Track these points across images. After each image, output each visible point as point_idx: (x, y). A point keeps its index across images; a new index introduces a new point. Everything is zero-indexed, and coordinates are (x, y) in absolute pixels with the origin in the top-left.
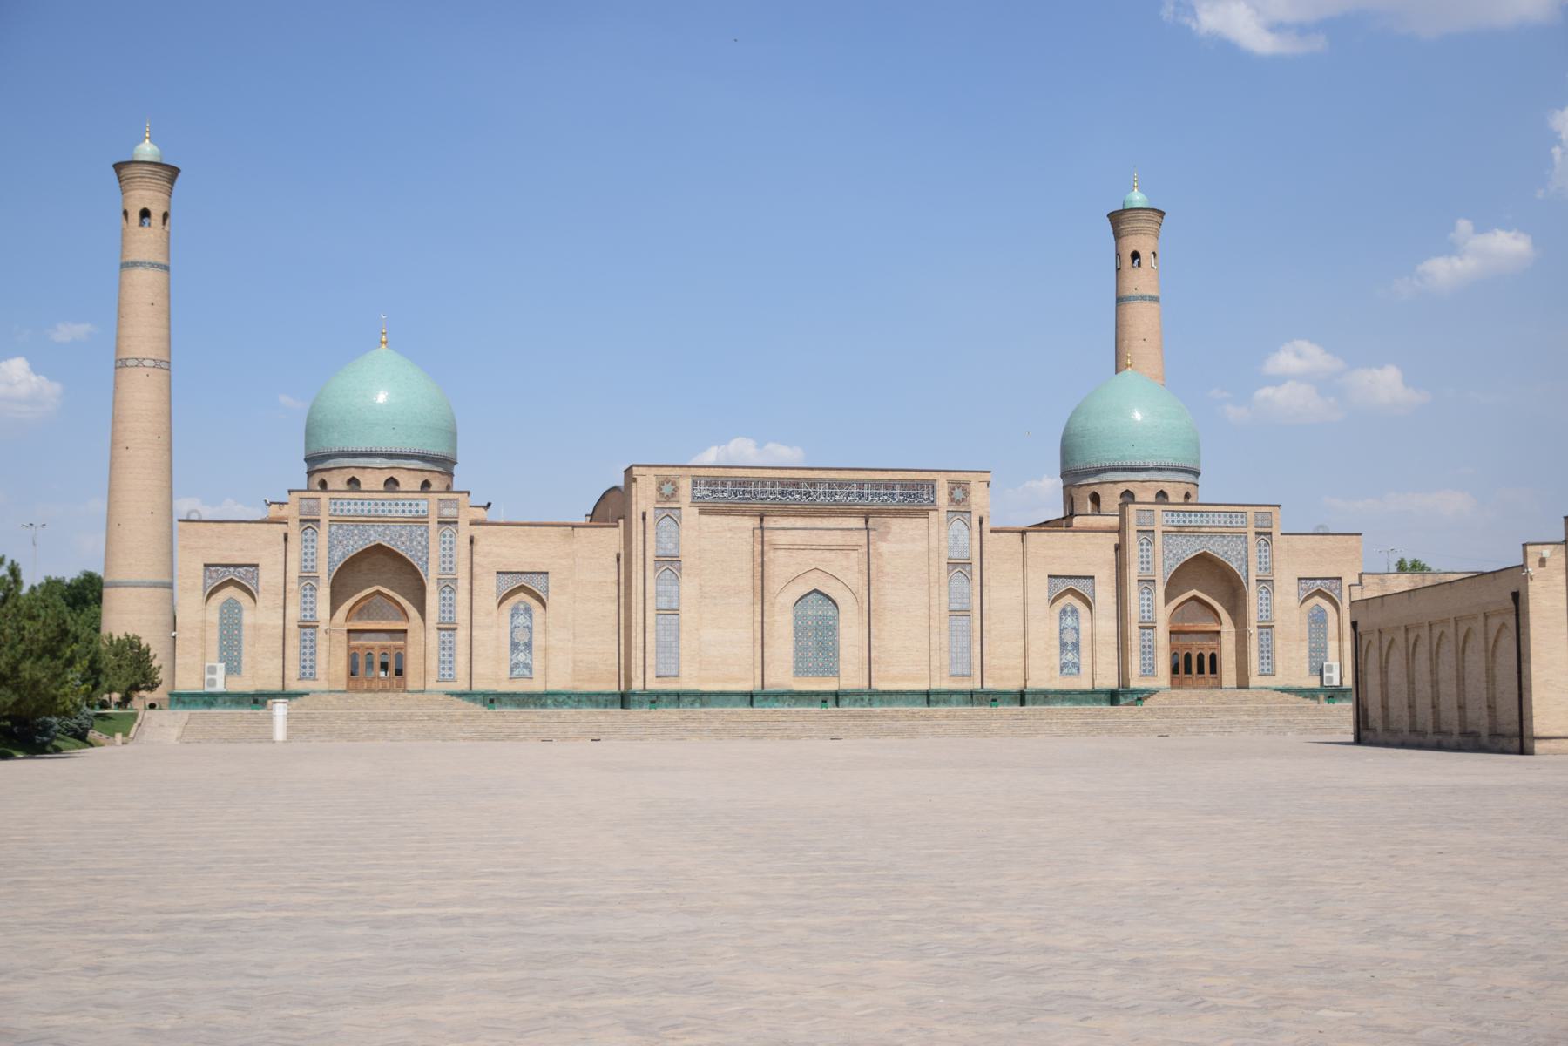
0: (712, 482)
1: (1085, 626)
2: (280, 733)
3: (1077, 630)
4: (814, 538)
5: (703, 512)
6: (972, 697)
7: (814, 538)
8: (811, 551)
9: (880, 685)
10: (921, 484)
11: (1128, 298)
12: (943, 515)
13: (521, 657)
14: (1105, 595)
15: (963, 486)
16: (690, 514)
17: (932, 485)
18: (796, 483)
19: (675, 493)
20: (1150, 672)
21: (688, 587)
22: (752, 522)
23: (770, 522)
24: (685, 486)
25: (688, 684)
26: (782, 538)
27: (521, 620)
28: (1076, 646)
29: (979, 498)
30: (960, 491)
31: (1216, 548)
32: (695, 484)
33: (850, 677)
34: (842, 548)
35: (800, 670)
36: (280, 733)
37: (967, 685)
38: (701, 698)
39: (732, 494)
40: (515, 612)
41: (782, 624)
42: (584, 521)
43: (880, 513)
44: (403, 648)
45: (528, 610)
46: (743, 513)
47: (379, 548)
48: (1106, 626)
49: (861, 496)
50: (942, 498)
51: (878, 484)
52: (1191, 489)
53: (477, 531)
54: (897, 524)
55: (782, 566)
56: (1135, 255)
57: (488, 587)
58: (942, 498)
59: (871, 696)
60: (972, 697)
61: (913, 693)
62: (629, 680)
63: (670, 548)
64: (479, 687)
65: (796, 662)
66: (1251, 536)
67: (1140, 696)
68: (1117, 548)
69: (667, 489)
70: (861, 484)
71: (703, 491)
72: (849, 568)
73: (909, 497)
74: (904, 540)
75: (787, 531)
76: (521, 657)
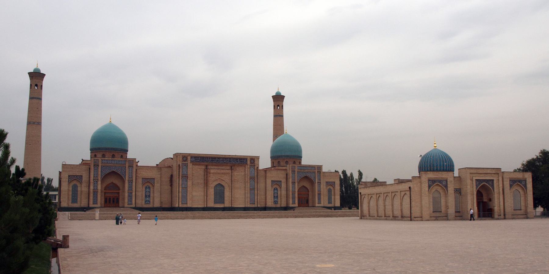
1: (279, 192)
3: (150, 192)
7: (219, 171)
8: (217, 175)
13: (148, 199)
14: (284, 185)
16: (190, 165)
20: (95, 202)
21: (190, 183)
24: (189, 158)
26: (212, 171)
28: (277, 197)
32: (191, 157)
33: (227, 204)
35: (215, 202)
37: (253, 206)
41: (211, 191)
48: (284, 192)
50: (249, 162)
55: (212, 178)
57: (140, 181)
58: (249, 162)
66: (127, 167)
67: (293, 208)
69: (185, 159)
75: (213, 170)
76: (148, 199)
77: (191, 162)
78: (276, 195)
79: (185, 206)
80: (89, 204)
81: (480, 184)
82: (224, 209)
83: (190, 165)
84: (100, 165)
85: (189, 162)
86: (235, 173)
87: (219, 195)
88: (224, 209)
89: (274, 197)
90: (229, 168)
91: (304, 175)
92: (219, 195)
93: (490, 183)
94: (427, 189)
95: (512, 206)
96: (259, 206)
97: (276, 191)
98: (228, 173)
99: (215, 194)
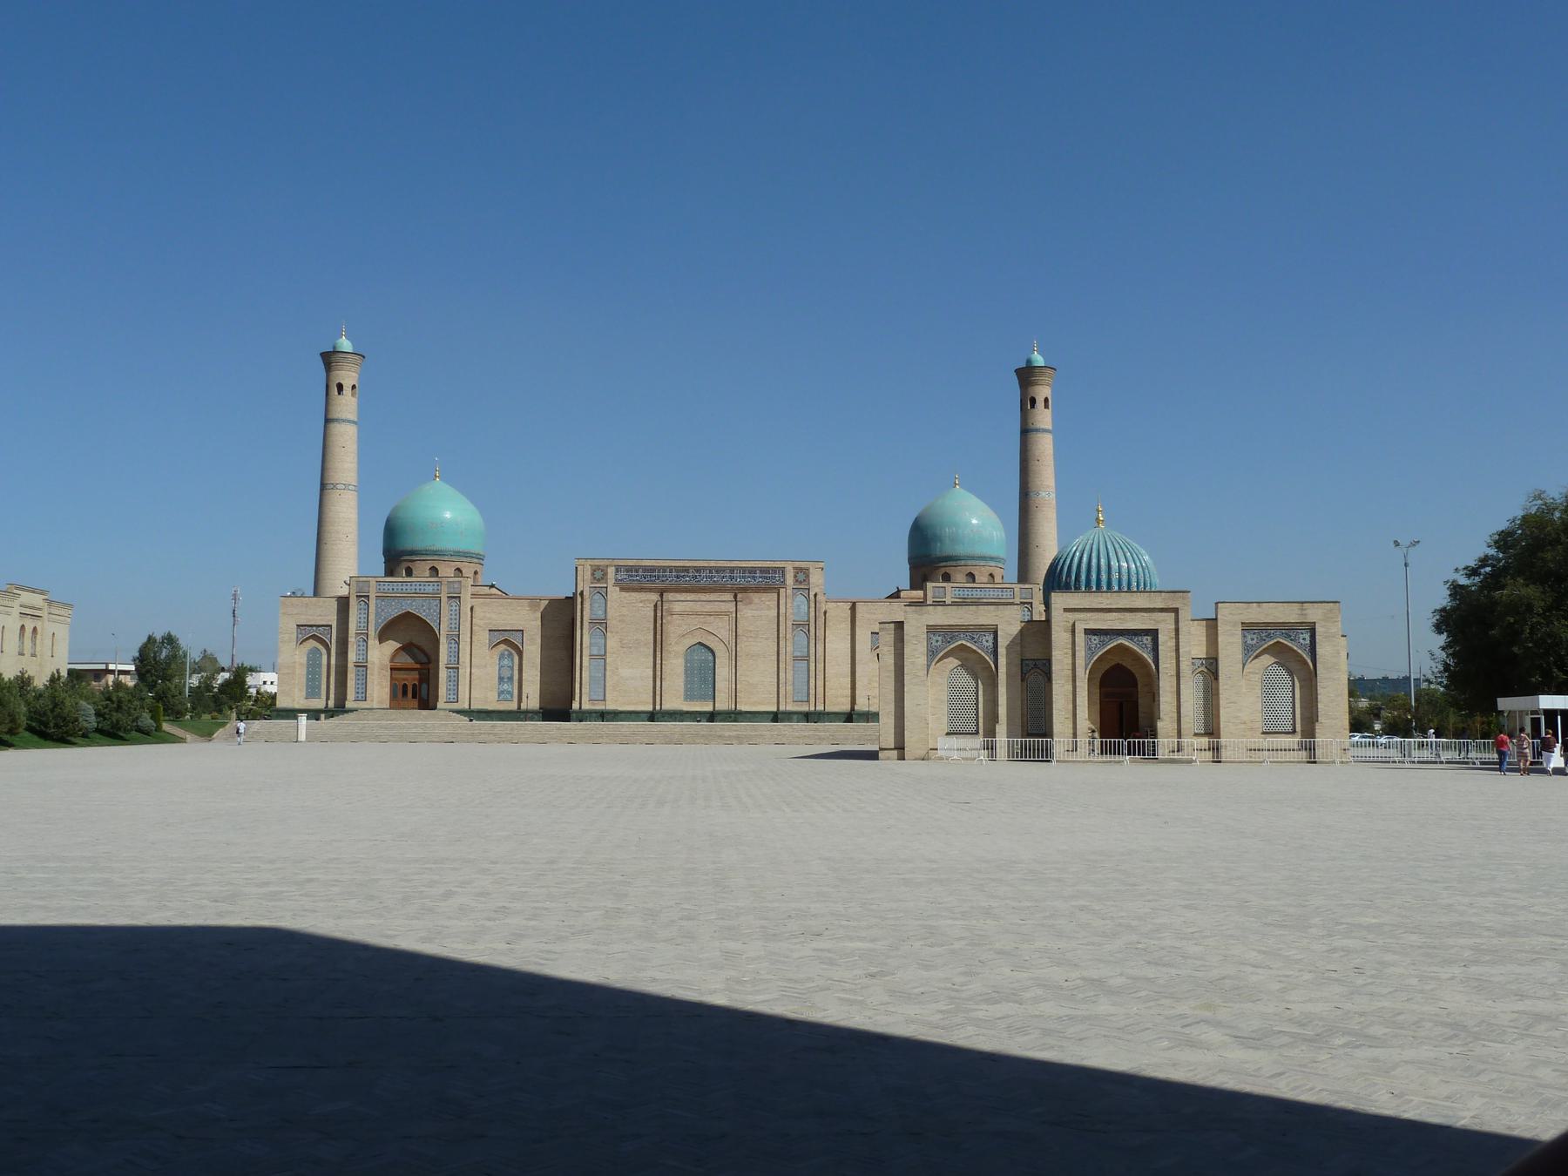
0: (629, 569)
2: (302, 737)
4: (698, 607)
5: (622, 589)
6: (808, 717)
7: (698, 607)
8: (692, 617)
9: (742, 707)
10: (775, 570)
11: (337, 420)
12: (789, 591)
13: (506, 687)
15: (805, 571)
16: (614, 593)
17: (783, 570)
18: (686, 569)
19: (604, 577)
21: (612, 642)
22: (655, 597)
23: (669, 596)
24: (611, 571)
25: (611, 706)
26: (677, 607)
27: (506, 662)
29: (816, 579)
30: (802, 574)
33: (723, 704)
34: (718, 614)
35: (689, 697)
36: (302, 737)
37: (805, 708)
38: (615, 716)
39: (639, 578)
40: (502, 657)
41: (675, 666)
43: (745, 590)
45: (510, 655)
46: (650, 590)
47: (408, 616)
49: (732, 578)
50: (790, 580)
51: (744, 569)
52: (478, 568)
53: (475, 602)
54: (755, 597)
56: (340, 387)
57: (483, 637)
58: (790, 580)
59: (734, 716)
60: (808, 717)
61: (700, 713)
62: (853, 702)
63: (600, 613)
65: (686, 691)
66: (444, 599)
69: (598, 574)
70: (732, 570)
72: (722, 628)
73: (766, 580)
74: (759, 611)
75: (680, 603)
76: (506, 687)
77: (618, 582)
78: (507, 674)
79: (599, 707)
80: (853, 702)
81: (1103, 644)
82: (712, 716)
83: (614, 593)
84: (372, 596)
85: (611, 581)
86: (746, 612)
87: (702, 672)
88: (712, 716)
89: (501, 679)
90: (729, 597)
91: (394, 611)
92: (702, 672)
93: (1147, 640)
94: (923, 660)
95: (1258, 717)
96: (523, 706)
97: (506, 662)
98: (726, 613)
99: (689, 672)
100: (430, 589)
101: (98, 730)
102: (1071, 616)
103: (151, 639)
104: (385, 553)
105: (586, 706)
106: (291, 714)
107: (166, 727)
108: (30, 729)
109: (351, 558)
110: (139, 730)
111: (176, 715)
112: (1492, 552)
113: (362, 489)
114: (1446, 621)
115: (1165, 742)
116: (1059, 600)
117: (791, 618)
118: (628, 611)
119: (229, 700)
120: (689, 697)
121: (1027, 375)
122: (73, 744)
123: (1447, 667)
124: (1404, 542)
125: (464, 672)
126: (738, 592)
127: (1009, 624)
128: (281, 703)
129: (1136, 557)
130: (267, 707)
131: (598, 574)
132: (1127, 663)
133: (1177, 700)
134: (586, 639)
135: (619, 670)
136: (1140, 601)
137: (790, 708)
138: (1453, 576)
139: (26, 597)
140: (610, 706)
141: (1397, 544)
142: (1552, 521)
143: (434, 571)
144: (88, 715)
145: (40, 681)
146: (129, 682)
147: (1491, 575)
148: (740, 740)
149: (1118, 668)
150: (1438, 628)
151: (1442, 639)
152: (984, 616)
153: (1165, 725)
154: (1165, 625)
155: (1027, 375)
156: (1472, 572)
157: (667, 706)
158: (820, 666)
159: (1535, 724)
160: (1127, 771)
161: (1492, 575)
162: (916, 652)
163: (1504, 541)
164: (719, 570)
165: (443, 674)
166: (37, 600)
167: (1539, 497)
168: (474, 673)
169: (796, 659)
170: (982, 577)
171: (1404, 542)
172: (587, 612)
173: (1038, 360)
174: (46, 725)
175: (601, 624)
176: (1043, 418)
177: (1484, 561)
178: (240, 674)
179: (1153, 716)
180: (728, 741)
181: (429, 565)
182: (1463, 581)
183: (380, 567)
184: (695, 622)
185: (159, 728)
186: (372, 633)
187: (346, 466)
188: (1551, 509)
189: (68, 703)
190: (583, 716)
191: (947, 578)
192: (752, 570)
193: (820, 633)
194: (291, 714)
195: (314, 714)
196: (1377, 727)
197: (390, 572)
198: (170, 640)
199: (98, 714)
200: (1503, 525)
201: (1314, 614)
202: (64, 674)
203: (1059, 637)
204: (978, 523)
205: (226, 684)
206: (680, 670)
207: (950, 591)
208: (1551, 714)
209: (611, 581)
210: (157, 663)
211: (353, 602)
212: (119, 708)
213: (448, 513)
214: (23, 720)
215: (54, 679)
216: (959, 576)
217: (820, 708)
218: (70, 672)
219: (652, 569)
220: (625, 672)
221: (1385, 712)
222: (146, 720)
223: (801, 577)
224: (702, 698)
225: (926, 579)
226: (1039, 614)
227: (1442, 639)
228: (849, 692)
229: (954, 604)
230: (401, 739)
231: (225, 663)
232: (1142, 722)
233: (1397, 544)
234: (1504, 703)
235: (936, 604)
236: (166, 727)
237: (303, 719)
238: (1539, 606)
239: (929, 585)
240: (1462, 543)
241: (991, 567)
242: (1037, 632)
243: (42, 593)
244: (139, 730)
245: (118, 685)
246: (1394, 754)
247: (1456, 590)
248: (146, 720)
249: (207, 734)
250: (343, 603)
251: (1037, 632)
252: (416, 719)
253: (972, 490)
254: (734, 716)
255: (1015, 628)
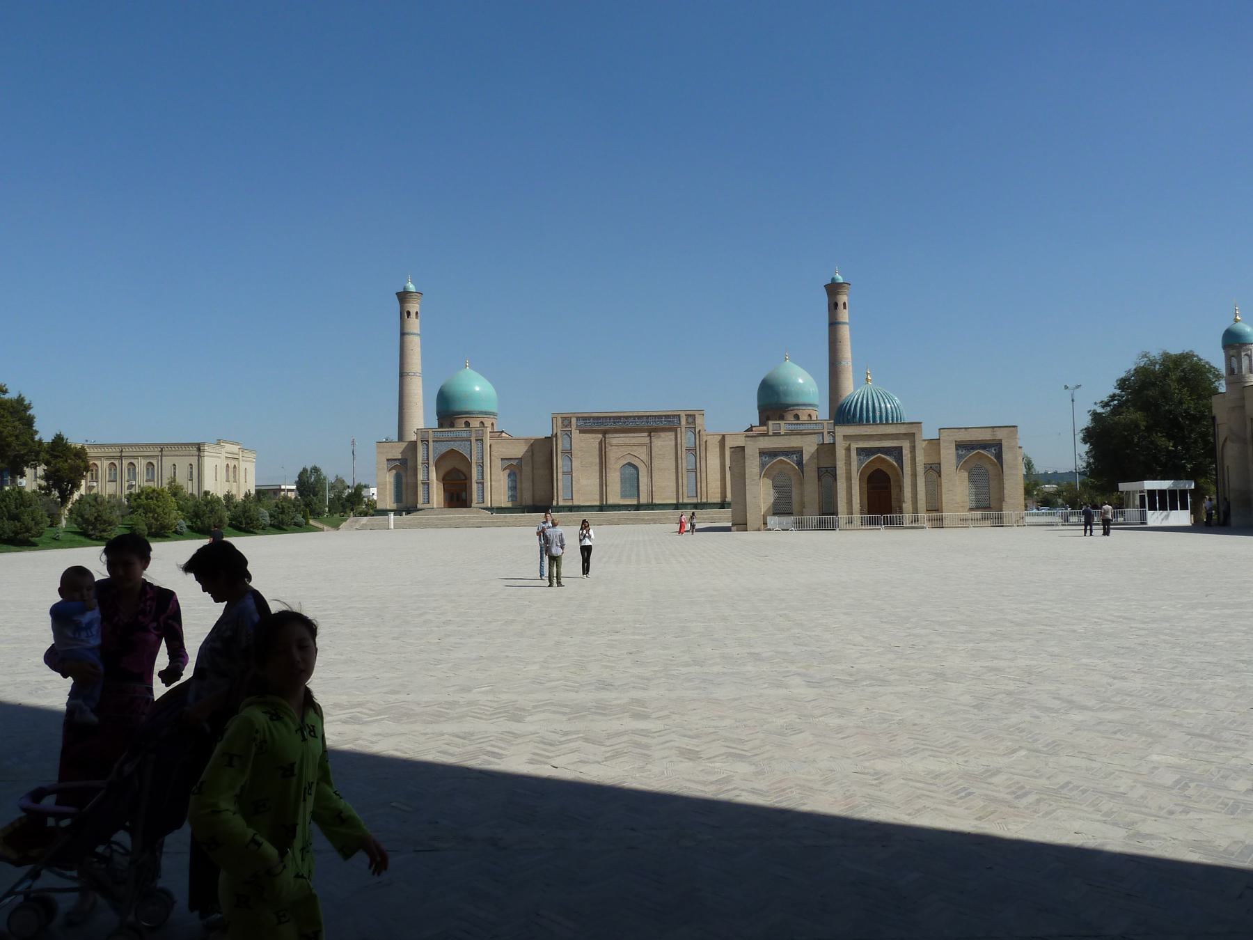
0: (584, 418)
4: (627, 441)
8: (623, 448)
9: (656, 501)
15: (693, 417)
16: (575, 434)
24: (574, 421)
26: (614, 441)
30: (691, 417)
31: (455, 446)
35: (623, 496)
37: (694, 501)
39: (604, 426)
41: (614, 478)
42: (1063, 452)
43: (656, 430)
44: (373, 510)
54: (663, 435)
55: (613, 454)
57: (498, 464)
62: (678, 498)
64: (495, 505)
68: (600, 443)
71: (581, 423)
72: (642, 453)
74: (664, 443)
75: (615, 439)
83: (575, 434)
85: (574, 427)
88: (638, 507)
91: (444, 448)
99: (623, 481)
100: (464, 435)
101: (271, 525)
102: (229, 462)
103: (305, 470)
104: (439, 413)
105: (561, 503)
106: (384, 512)
107: (311, 522)
108: (230, 525)
109: (421, 417)
110: (296, 524)
111: (317, 514)
112: (1118, 391)
113: (425, 376)
114: (1090, 436)
115: (907, 516)
116: (842, 431)
117: (684, 445)
118: (585, 444)
119: (351, 503)
120: (623, 496)
121: (403, 296)
122: (256, 534)
123: (1089, 464)
124: (1071, 385)
125: (488, 484)
126: (651, 431)
127: (809, 446)
128: (380, 506)
129: (891, 400)
130: (373, 510)
131: (566, 422)
132: (884, 468)
133: (913, 488)
134: (560, 463)
135: (580, 479)
136: (890, 430)
137: (686, 501)
138: (1093, 408)
139: (229, 447)
140: (576, 503)
141: (1066, 387)
142: (1153, 372)
143: (467, 424)
144: (264, 514)
145: (240, 497)
146: (292, 495)
147: (1117, 405)
148: (654, 521)
149: (878, 471)
150: (1085, 441)
151: (1087, 447)
152: (795, 442)
153: (907, 505)
154: (906, 445)
155: (833, 289)
156: (1106, 405)
157: (610, 502)
158: (704, 475)
159: (1142, 498)
160: (882, 538)
161: (1120, 406)
162: (753, 465)
163: (1122, 384)
164: (639, 417)
165: (475, 486)
166: (235, 448)
167: (1145, 356)
168: (494, 485)
169: (688, 471)
170: (804, 417)
171: (1071, 385)
172: (561, 444)
173: (411, 287)
174: (241, 523)
175: (569, 453)
176: (414, 325)
177: (1113, 397)
178: (359, 489)
179: (900, 501)
180: (647, 522)
181: (463, 421)
182: (1100, 410)
183: (434, 423)
184: (627, 450)
185: (307, 523)
186: (431, 462)
187: (415, 362)
188: (1153, 363)
189: (172, 516)
190: (559, 509)
191: (782, 418)
192: (660, 417)
193: (703, 454)
194: (384, 512)
195: (398, 512)
196: (1060, 501)
197: (441, 425)
198: (316, 470)
199: (271, 516)
200: (1123, 375)
201: (1000, 435)
202: (253, 492)
203: (840, 453)
204: (805, 383)
205: (350, 495)
206: (618, 479)
207: (783, 426)
208: (1152, 493)
209: (574, 427)
210: (309, 485)
211: (420, 445)
212: (283, 512)
213: (477, 388)
214: (227, 520)
215: (247, 496)
216: (790, 417)
217: (704, 500)
218: (258, 492)
219: (598, 418)
220: (584, 482)
221: (1048, 496)
222: (300, 518)
223: (690, 420)
224: (631, 496)
225: (768, 419)
226: (828, 440)
227: (1087, 447)
228: (674, 489)
229: (786, 434)
230: (450, 526)
231: (349, 483)
232: (894, 504)
233: (1066, 387)
234: (1123, 487)
235: (775, 434)
236: (311, 522)
237: (392, 515)
238: (1143, 425)
239: (770, 423)
240: (1099, 388)
241: (809, 410)
242: (827, 450)
243: (238, 444)
244: (296, 524)
245: (286, 498)
246: (1057, 519)
247: (1096, 416)
248: (300, 518)
249: (337, 527)
250: (413, 445)
251: (827, 450)
252: (458, 514)
253: (476, 370)
254: (651, 506)
255: (813, 448)
